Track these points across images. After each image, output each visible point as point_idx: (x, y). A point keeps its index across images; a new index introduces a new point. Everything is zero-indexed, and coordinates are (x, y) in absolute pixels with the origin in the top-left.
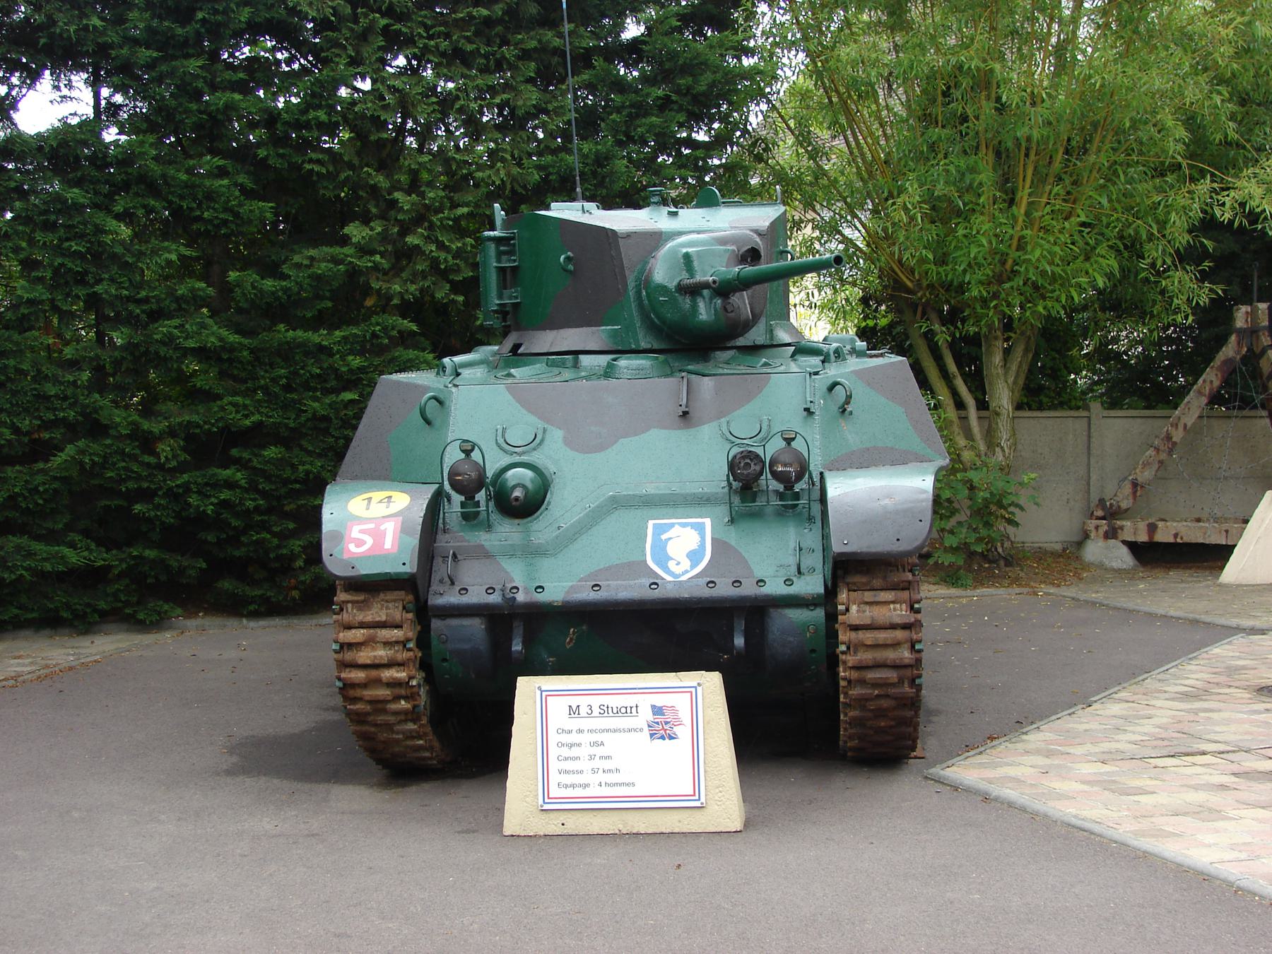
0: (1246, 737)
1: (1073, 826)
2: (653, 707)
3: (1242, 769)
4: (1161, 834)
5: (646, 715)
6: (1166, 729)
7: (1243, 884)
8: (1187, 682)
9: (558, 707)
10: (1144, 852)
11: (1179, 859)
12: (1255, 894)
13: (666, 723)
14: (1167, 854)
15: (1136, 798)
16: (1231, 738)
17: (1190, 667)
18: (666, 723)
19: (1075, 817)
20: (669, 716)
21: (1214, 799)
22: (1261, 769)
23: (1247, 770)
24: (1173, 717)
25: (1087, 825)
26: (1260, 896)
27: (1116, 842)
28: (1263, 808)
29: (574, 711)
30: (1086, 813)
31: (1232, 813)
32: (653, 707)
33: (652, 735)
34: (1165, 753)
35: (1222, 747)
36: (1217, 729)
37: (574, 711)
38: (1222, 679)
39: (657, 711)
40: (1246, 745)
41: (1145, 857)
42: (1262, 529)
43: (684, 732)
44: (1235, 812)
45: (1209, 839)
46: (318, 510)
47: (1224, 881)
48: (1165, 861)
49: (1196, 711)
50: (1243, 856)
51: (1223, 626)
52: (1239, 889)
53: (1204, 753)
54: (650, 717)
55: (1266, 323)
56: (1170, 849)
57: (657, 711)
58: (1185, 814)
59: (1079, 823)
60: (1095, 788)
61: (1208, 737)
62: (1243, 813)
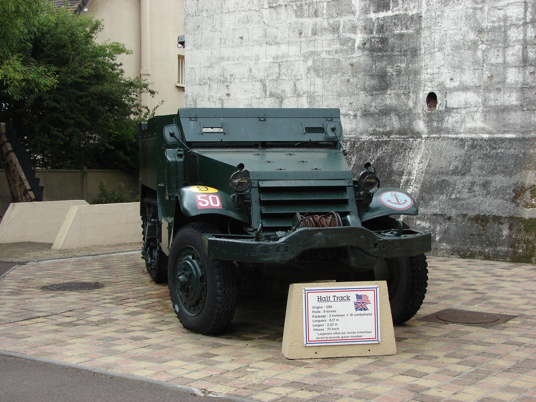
0: (53, 309)
1: (5, 355)
2: (357, 295)
3: (59, 323)
4: (46, 354)
5: (353, 299)
6: (16, 308)
7: (96, 371)
8: (10, 287)
9: (313, 298)
10: (45, 363)
11: (62, 364)
12: (102, 374)
13: (363, 303)
14: (56, 362)
15: (25, 339)
16: (47, 309)
17: (5, 281)
18: (363, 303)
19: (4, 351)
20: (364, 300)
21: (58, 336)
22: (66, 322)
23: (61, 322)
24: (15, 303)
25: (12, 354)
26: (105, 375)
27: (29, 360)
28: (80, 338)
29: (320, 299)
30: (8, 349)
31: (70, 341)
32: (357, 295)
33: (356, 309)
34: (22, 318)
35: (45, 314)
36: (37, 306)
37: (320, 299)
38: (23, 285)
39: (359, 297)
40: (55, 312)
41: (45, 365)
42: (10, 220)
43: (371, 307)
44: (70, 341)
45: (69, 353)
46: (82, 199)
47: (86, 370)
48: (55, 365)
49: (24, 299)
50: (88, 359)
51: (5, 262)
52: (94, 373)
53: (39, 317)
54: (356, 300)
55: (4, 131)
56: (56, 360)
57: (359, 297)
58: (51, 344)
59: (8, 354)
60: (3, 337)
61: (37, 310)
62: (75, 340)
